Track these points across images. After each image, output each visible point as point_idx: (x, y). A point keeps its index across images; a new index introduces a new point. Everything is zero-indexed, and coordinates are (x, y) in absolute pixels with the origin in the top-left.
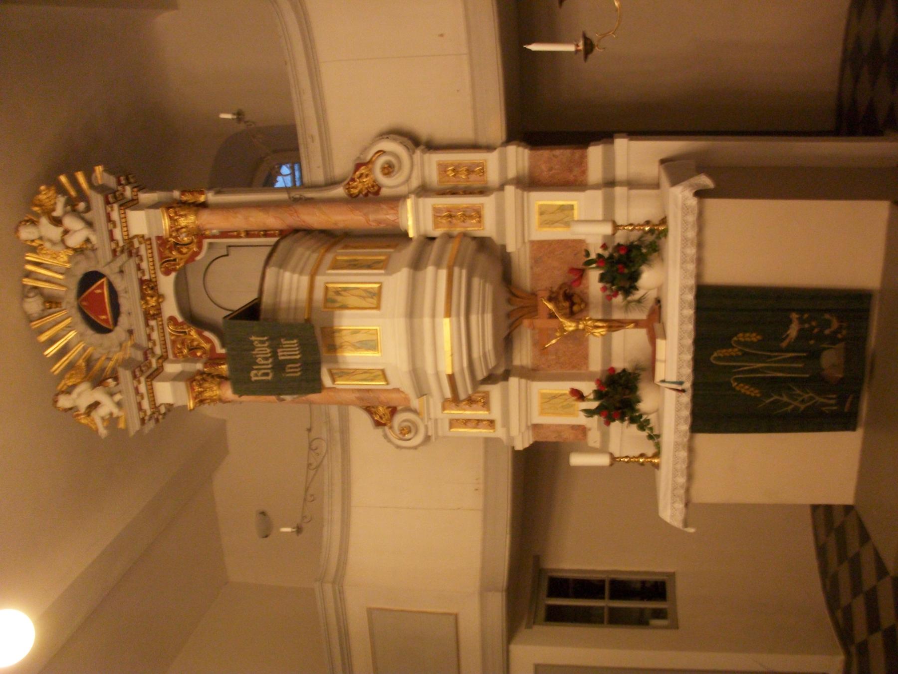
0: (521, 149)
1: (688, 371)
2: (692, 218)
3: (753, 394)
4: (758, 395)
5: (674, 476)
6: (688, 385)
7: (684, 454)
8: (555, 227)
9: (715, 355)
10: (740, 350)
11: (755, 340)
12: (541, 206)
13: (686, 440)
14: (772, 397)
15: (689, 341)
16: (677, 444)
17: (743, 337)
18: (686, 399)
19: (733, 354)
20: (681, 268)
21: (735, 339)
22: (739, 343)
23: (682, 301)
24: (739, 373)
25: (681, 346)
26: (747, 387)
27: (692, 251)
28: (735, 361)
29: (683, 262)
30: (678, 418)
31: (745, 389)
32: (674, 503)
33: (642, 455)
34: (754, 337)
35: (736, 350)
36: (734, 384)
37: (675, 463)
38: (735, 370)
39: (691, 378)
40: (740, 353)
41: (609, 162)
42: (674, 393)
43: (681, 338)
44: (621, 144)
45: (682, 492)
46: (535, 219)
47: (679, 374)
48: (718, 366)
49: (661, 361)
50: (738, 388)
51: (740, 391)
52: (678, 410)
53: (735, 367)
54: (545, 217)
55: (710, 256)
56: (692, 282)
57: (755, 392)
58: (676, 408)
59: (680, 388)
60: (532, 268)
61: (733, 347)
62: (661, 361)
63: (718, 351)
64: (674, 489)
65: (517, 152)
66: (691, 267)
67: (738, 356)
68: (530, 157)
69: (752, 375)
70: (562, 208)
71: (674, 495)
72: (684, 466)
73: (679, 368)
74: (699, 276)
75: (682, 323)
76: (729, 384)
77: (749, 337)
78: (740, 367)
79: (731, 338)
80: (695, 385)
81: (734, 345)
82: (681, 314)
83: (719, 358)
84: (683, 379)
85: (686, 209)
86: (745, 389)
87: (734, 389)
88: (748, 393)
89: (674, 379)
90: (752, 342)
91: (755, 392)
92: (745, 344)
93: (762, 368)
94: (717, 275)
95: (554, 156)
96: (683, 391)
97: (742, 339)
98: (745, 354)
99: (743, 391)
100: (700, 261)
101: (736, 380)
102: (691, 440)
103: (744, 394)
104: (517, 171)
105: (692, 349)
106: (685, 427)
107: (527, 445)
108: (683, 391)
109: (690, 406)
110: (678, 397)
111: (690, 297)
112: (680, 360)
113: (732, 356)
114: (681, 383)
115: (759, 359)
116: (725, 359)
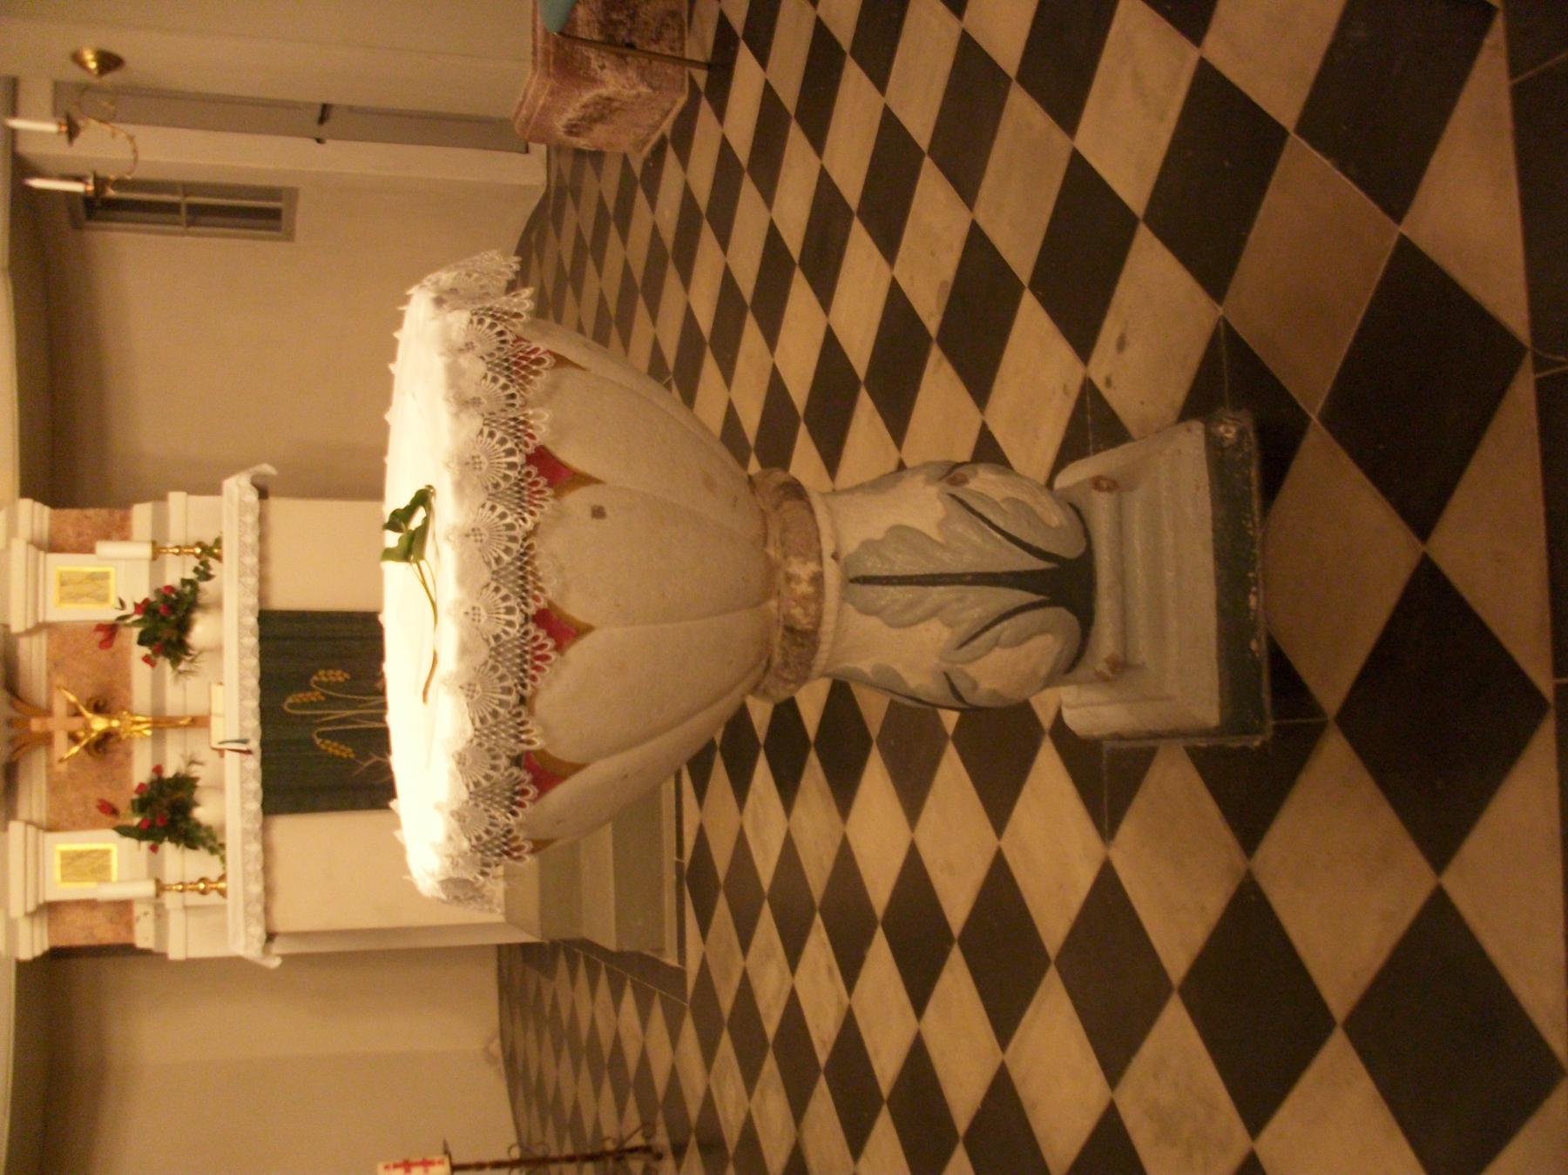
0: (38, 505)
1: (253, 723)
2: (251, 519)
3: (345, 755)
4: (352, 756)
5: (245, 883)
6: (254, 745)
7: (255, 847)
8: (83, 603)
9: (290, 700)
10: (323, 694)
11: (341, 679)
12: (61, 574)
13: (258, 826)
14: (370, 758)
15: (253, 682)
16: (245, 832)
17: (326, 676)
18: (253, 763)
19: (314, 699)
20: (240, 582)
21: (315, 678)
22: (319, 684)
23: (241, 626)
24: (322, 724)
25: (242, 688)
26: (335, 744)
27: (252, 560)
28: (316, 709)
29: (241, 575)
30: (244, 793)
31: (332, 748)
32: (247, 926)
33: (202, 880)
34: (340, 676)
35: (317, 693)
36: (318, 741)
37: (245, 864)
38: (317, 721)
39: (259, 732)
40: (323, 698)
41: (160, 523)
42: (237, 755)
43: (242, 678)
44: (176, 499)
45: (259, 909)
46: (52, 590)
47: (242, 729)
48: (296, 716)
49: (218, 715)
50: (323, 747)
51: (326, 751)
52: (243, 782)
53: (316, 716)
54: (70, 588)
55: (276, 570)
56: (253, 601)
57: (347, 752)
58: (241, 777)
59: (243, 747)
60: (49, 674)
61: (313, 690)
62: (218, 715)
63: (294, 695)
64: (247, 904)
65: (33, 507)
66: (252, 581)
67: (319, 701)
68: (51, 518)
69: (341, 727)
70: (92, 577)
71: (247, 914)
72: (259, 867)
73: (242, 719)
74: (262, 598)
75: (241, 657)
76: (312, 742)
77: (334, 675)
78: (323, 716)
79: (310, 676)
80: (264, 744)
81: (314, 686)
82: (240, 644)
83: (293, 706)
84: (248, 735)
85: (243, 508)
86: (332, 748)
87: (317, 749)
88: (337, 753)
89: (237, 737)
90: (337, 683)
91: (347, 752)
92: (328, 686)
93: (354, 716)
94: (286, 598)
95: (86, 517)
96: (249, 752)
97: (324, 679)
98: (329, 698)
99: (331, 750)
100: (263, 580)
101: (320, 735)
102: (265, 828)
103: (333, 756)
104: (33, 534)
105: (257, 692)
106: (255, 806)
107: (38, 952)
108: (249, 752)
109: (259, 774)
110: (242, 762)
111: (252, 621)
112: (241, 707)
113: (312, 702)
114: (244, 742)
115: (350, 704)
116: (303, 706)
